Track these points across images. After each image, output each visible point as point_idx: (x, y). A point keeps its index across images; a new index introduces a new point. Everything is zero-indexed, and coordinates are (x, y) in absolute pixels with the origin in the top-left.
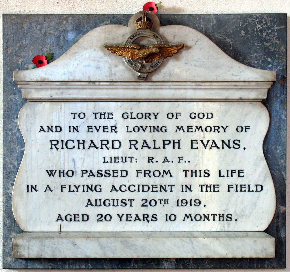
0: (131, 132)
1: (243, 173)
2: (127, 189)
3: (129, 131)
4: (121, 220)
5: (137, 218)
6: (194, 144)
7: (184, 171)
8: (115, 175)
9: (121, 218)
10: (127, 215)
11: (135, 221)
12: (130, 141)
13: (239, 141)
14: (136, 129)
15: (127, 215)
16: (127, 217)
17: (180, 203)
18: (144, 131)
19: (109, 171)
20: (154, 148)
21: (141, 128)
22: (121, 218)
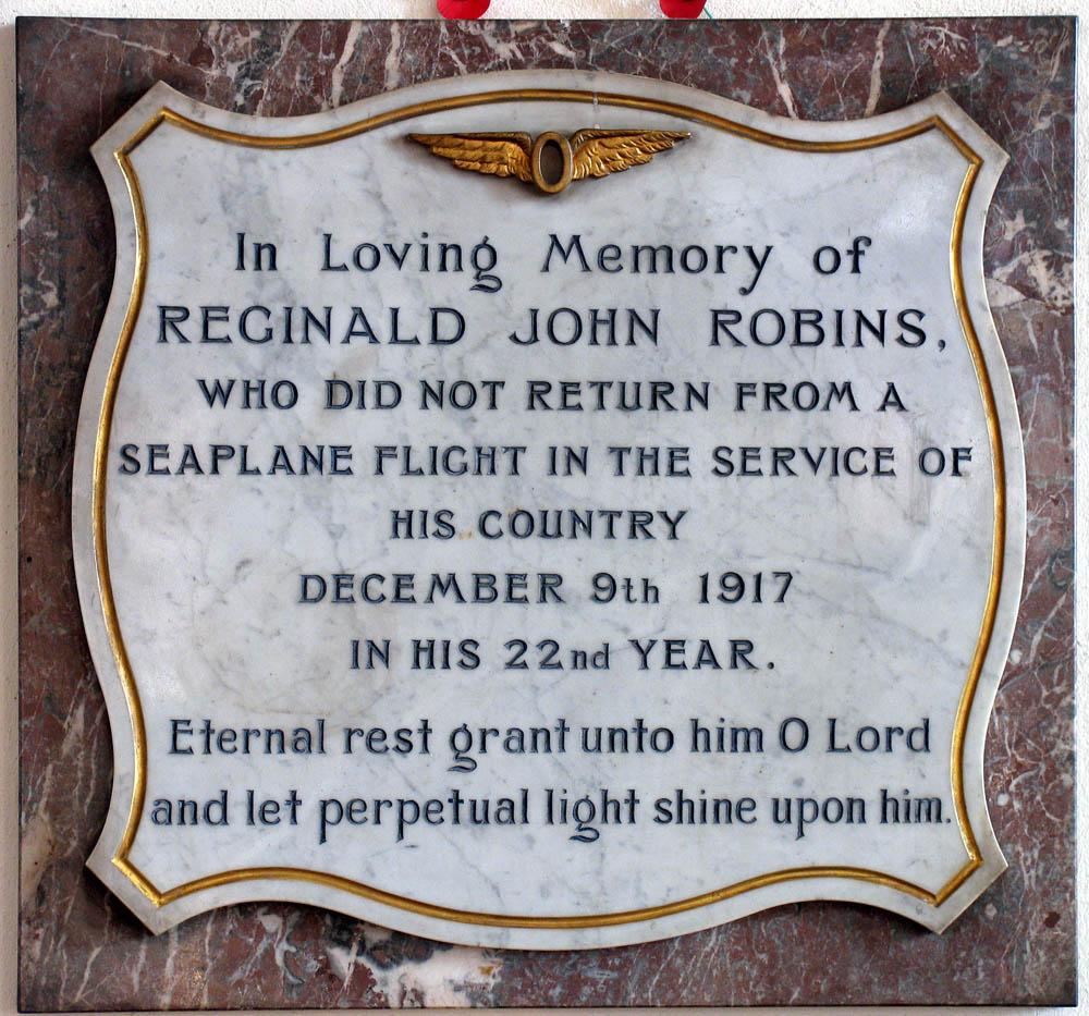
0: (344, 268)
1: (350, 457)
2: (506, 530)
3: (333, 263)
4: (645, 665)
5: (707, 655)
6: (212, 324)
7: (612, 450)
8: (752, 465)
9: (644, 654)
10: (669, 643)
11: (698, 666)
12: (716, 313)
13: (921, 315)
14: (367, 258)
15: (669, 643)
16: (669, 651)
17: (714, 589)
18: (399, 261)
19: (730, 451)
20: (395, 339)
21: (591, 259)
22: (644, 654)
